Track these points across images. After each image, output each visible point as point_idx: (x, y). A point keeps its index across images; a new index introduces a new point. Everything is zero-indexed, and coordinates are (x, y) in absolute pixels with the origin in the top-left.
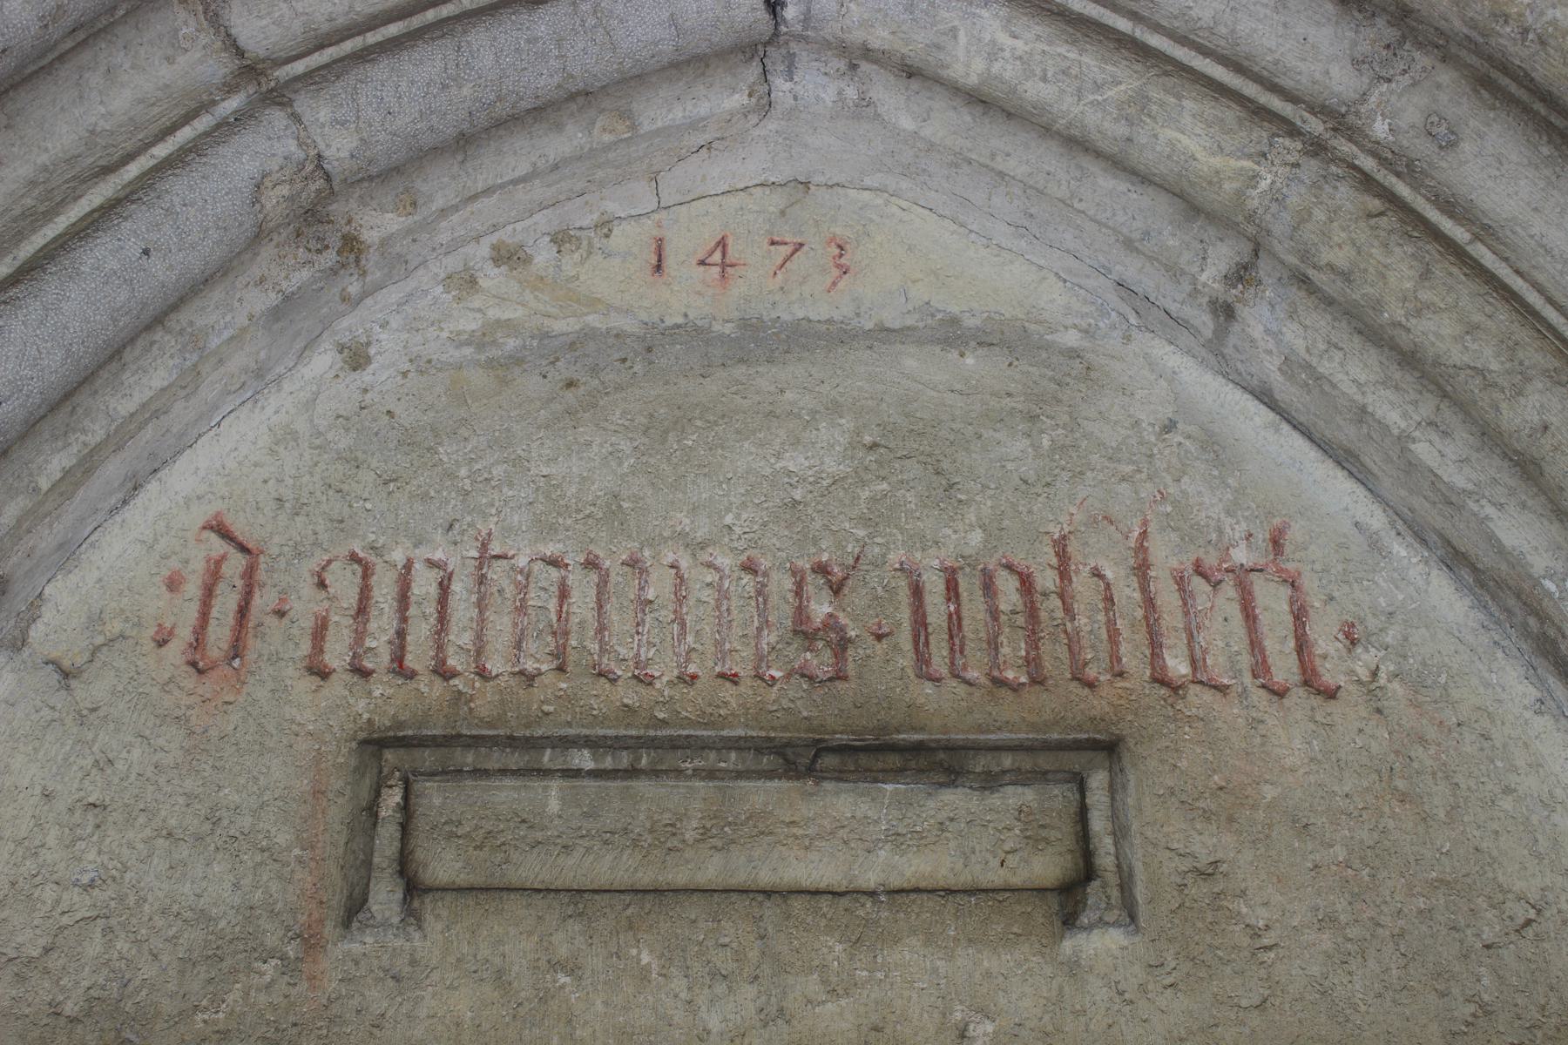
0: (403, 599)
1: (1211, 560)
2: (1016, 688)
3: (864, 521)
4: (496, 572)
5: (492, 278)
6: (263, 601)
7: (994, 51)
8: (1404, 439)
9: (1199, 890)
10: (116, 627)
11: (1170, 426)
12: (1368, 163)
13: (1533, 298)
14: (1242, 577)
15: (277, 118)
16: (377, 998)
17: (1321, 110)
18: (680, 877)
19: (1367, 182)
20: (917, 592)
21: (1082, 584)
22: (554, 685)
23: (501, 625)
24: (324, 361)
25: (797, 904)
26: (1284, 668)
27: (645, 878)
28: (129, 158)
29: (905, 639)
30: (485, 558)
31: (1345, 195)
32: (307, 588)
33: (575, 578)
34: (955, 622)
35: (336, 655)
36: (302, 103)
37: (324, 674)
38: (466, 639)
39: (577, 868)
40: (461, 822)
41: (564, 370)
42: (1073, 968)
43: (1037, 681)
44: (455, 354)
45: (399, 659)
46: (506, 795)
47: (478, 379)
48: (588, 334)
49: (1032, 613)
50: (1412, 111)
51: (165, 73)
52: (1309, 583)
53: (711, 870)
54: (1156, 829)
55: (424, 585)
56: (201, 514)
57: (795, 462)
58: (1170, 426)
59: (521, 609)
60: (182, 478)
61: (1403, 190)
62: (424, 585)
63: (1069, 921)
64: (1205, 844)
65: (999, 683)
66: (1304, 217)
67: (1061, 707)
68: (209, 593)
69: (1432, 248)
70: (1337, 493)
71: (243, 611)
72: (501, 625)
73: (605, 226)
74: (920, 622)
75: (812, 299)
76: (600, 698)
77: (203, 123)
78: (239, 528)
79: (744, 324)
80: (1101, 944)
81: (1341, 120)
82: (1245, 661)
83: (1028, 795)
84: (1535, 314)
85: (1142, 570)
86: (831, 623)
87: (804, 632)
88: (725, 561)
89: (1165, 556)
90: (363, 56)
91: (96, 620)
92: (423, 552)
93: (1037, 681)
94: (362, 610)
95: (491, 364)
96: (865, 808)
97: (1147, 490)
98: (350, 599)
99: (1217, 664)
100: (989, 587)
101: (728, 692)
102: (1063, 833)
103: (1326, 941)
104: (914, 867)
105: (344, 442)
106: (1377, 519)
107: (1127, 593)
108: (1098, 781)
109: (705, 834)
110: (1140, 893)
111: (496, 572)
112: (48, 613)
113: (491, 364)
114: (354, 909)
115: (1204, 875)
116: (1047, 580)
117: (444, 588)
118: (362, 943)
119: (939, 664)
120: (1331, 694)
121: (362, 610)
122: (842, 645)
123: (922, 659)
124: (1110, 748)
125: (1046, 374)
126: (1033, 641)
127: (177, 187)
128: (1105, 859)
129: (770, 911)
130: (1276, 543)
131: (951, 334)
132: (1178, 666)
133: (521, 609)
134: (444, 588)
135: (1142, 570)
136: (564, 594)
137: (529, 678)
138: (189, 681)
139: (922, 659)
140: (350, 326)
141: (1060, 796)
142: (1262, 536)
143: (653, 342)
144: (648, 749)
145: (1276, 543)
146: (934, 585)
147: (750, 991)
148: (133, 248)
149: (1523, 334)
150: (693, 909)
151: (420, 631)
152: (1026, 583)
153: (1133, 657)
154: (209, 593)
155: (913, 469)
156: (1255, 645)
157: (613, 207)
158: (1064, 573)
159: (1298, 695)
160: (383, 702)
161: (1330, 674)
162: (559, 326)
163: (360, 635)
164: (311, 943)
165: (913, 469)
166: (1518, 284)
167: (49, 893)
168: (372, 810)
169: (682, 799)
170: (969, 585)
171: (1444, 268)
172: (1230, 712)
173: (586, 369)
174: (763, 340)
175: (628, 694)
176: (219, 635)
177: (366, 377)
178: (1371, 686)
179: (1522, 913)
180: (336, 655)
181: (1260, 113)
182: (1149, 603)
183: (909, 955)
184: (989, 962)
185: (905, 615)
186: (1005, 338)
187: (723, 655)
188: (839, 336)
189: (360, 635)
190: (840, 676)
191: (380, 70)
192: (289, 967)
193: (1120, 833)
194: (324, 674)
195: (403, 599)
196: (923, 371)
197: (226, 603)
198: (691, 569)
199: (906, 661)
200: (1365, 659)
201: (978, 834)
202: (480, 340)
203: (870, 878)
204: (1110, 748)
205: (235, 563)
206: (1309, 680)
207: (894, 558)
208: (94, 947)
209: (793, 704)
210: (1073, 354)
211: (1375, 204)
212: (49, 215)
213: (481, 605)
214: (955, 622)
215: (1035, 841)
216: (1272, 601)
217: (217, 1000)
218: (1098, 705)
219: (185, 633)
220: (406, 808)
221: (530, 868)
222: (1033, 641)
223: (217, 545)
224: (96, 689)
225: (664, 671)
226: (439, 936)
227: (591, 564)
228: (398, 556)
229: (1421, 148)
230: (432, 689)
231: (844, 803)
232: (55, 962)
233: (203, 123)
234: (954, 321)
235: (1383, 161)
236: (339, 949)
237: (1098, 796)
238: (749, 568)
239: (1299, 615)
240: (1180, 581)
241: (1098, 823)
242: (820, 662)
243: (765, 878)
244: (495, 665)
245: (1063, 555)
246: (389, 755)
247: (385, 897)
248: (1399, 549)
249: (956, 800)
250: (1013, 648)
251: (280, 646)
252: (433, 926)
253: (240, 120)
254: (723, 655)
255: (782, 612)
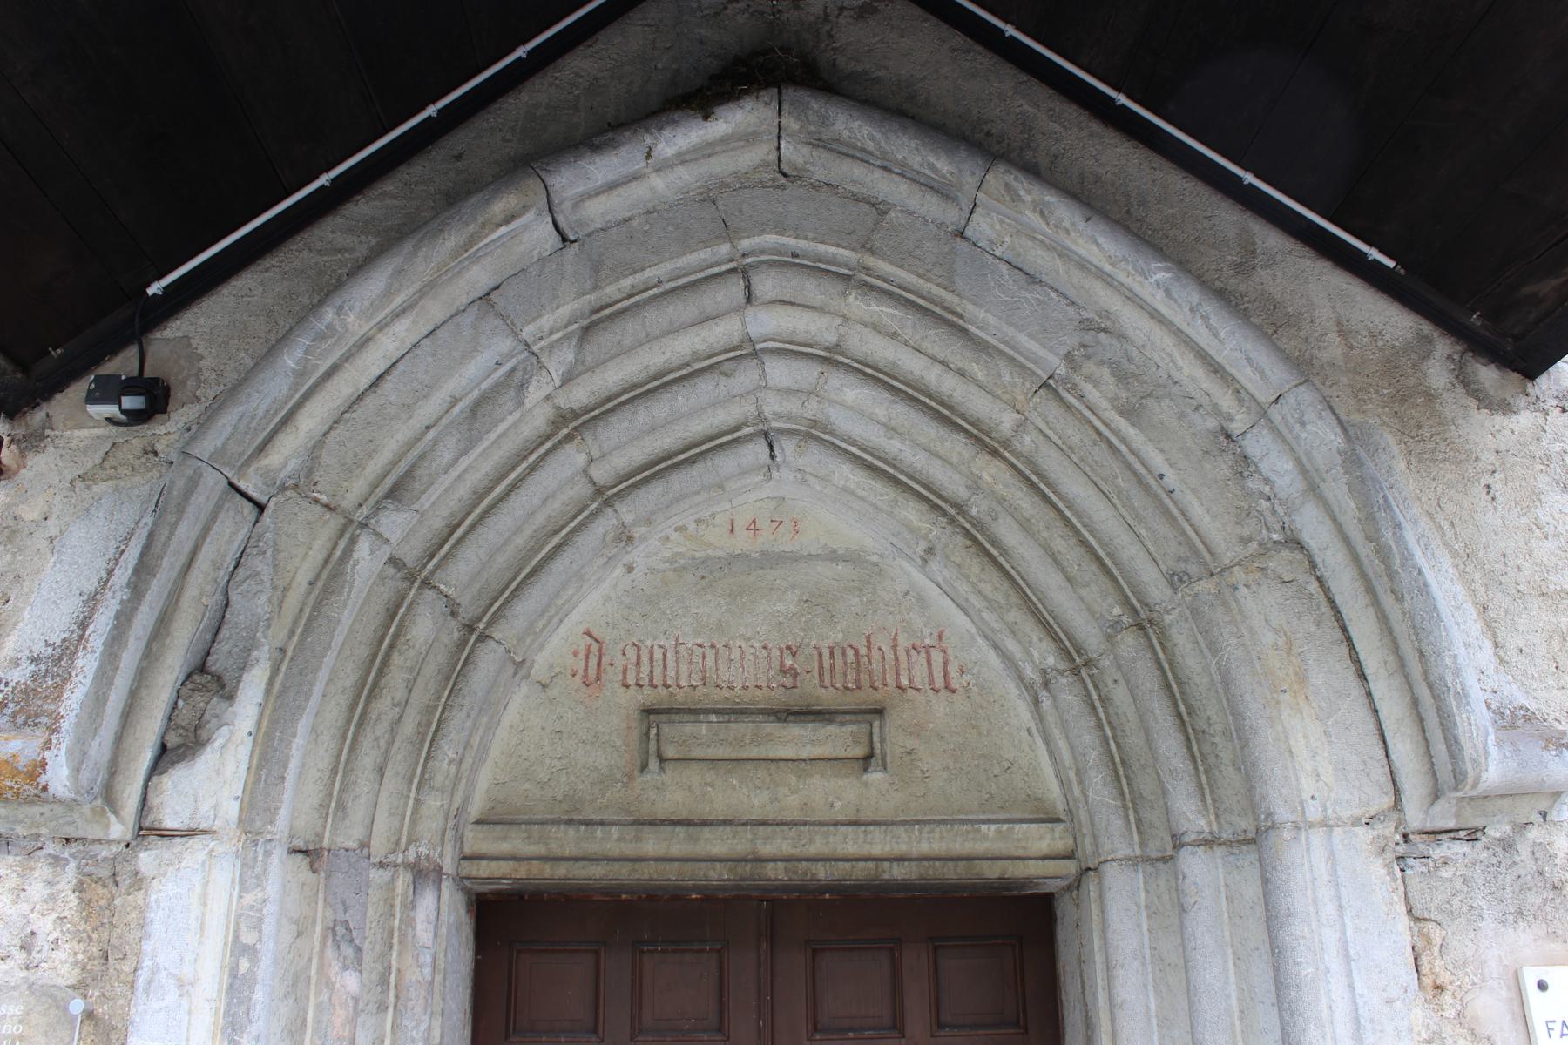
0: (651, 659)
1: (918, 643)
2: (851, 690)
3: (803, 630)
4: (682, 649)
5: (675, 536)
6: (605, 660)
7: (847, 480)
8: (980, 611)
9: (907, 759)
10: (557, 670)
11: (907, 593)
12: (968, 526)
13: (1017, 577)
14: (928, 649)
15: (609, 511)
16: (652, 795)
17: (955, 505)
18: (744, 755)
19: (967, 534)
20: (820, 655)
21: (875, 653)
22: (702, 690)
23: (684, 669)
24: (619, 570)
25: (781, 764)
26: (939, 683)
27: (734, 755)
28: (563, 527)
29: (816, 673)
30: (678, 644)
31: (960, 540)
32: (619, 654)
33: (708, 651)
34: (833, 666)
35: (631, 680)
36: (617, 505)
37: (628, 687)
38: (673, 674)
39: (712, 752)
40: (676, 734)
41: (701, 572)
42: (866, 784)
43: (859, 688)
44: (662, 566)
45: (651, 680)
46: (689, 728)
47: (671, 575)
48: (708, 558)
49: (858, 663)
50: (984, 507)
51: (571, 493)
52: (950, 651)
53: (754, 753)
54: (894, 737)
55: (658, 654)
56: (582, 629)
57: (780, 607)
58: (907, 593)
59: (690, 663)
60: (575, 616)
61: (979, 536)
62: (658, 654)
63: (866, 770)
64: (910, 743)
65: (847, 688)
66: (946, 546)
67: (866, 698)
68: (587, 658)
69: (986, 559)
70: (961, 619)
71: (599, 664)
72: (684, 669)
73: (713, 516)
74: (821, 667)
75: (786, 545)
76: (718, 695)
77: (585, 514)
78: (595, 633)
79: (763, 553)
80: (875, 776)
81: (960, 507)
82: (927, 680)
83: (854, 727)
84: (1017, 583)
85: (895, 647)
86: (792, 668)
87: (784, 671)
88: (757, 645)
89: (903, 642)
90: (636, 486)
91: (551, 667)
92: (656, 643)
93: (859, 688)
94: (638, 663)
95: (675, 570)
96: (802, 732)
97: (898, 617)
98: (634, 660)
99: (917, 682)
100: (844, 654)
101: (758, 693)
102: (865, 740)
103: (945, 775)
104: (818, 751)
105: (628, 601)
106: (973, 630)
107: (889, 655)
108: (876, 724)
109: (752, 741)
110: (888, 760)
111: (682, 649)
112: (536, 666)
113: (675, 570)
114: (644, 767)
115: (909, 753)
116: (863, 651)
117: (665, 655)
118: (647, 778)
119: (827, 683)
120: (953, 691)
121: (638, 663)
122: (796, 675)
123: (821, 680)
124: (880, 712)
125: (865, 570)
126: (858, 674)
127: (580, 539)
128: (877, 751)
129: (773, 766)
130: (940, 637)
131: (833, 557)
132: (905, 682)
133: (690, 663)
134: (665, 655)
135: (895, 647)
136: (704, 657)
137: (694, 687)
138: (584, 689)
139: (821, 680)
140: (627, 559)
141: (864, 727)
142: (935, 635)
143: (733, 559)
144: (735, 712)
145: (940, 637)
146: (826, 653)
147: (766, 792)
148: (567, 561)
149: (1011, 592)
150: (749, 766)
151: (658, 671)
152: (856, 652)
153: (890, 680)
154: (587, 658)
155: (820, 610)
156: (930, 674)
157: (716, 509)
158: (869, 649)
159: (943, 692)
160: (647, 696)
161: (954, 684)
162: (698, 555)
163: (638, 672)
164: (631, 778)
165: (820, 610)
166: (1012, 572)
167: (548, 761)
168: (647, 734)
169: (745, 728)
170: (837, 653)
171: (989, 567)
172: (921, 698)
173: (709, 571)
174: (771, 559)
175: (727, 693)
176: (592, 672)
177: (633, 576)
178: (967, 689)
179: (1007, 765)
180: (631, 680)
181: (935, 507)
182: (897, 659)
183: (816, 780)
184: (840, 782)
185: (816, 664)
186: (852, 558)
187: (757, 679)
188: (795, 558)
189: (638, 672)
190: (795, 687)
191: (642, 492)
192: (625, 785)
193: (883, 741)
194: (628, 687)
195: (651, 659)
196: (825, 572)
197: (593, 661)
198: (741, 647)
199: (816, 681)
200: (967, 677)
201: (837, 740)
202: (671, 561)
203: (804, 755)
204: (880, 712)
205: (595, 647)
206: (947, 687)
207: (813, 643)
208: (564, 779)
209: (779, 697)
210: (876, 564)
211: (969, 543)
212: (540, 549)
213: (677, 662)
214: (833, 666)
215: (856, 743)
216: (937, 658)
217: (604, 796)
218: (878, 696)
219: (581, 672)
220: (658, 735)
221: (697, 753)
222: (858, 674)
223: (589, 640)
224: (554, 692)
225: (738, 685)
226: (670, 775)
227: (713, 646)
228: (649, 643)
229: (986, 519)
230: (662, 691)
231: (795, 730)
232: (552, 783)
233: (585, 514)
234: (835, 551)
235: (973, 525)
236: (639, 780)
237: (876, 730)
238: (765, 648)
239: (945, 663)
240: (907, 652)
241: (876, 738)
242: (788, 682)
243: (771, 755)
244: (683, 683)
245: (869, 642)
246: (652, 717)
247: (653, 764)
248: (980, 640)
249: (832, 729)
250: (851, 676)
251: (612, 676)
252: (669, 772)
253: (595, 514)
254: (757, 679)
255: (776, 664)
